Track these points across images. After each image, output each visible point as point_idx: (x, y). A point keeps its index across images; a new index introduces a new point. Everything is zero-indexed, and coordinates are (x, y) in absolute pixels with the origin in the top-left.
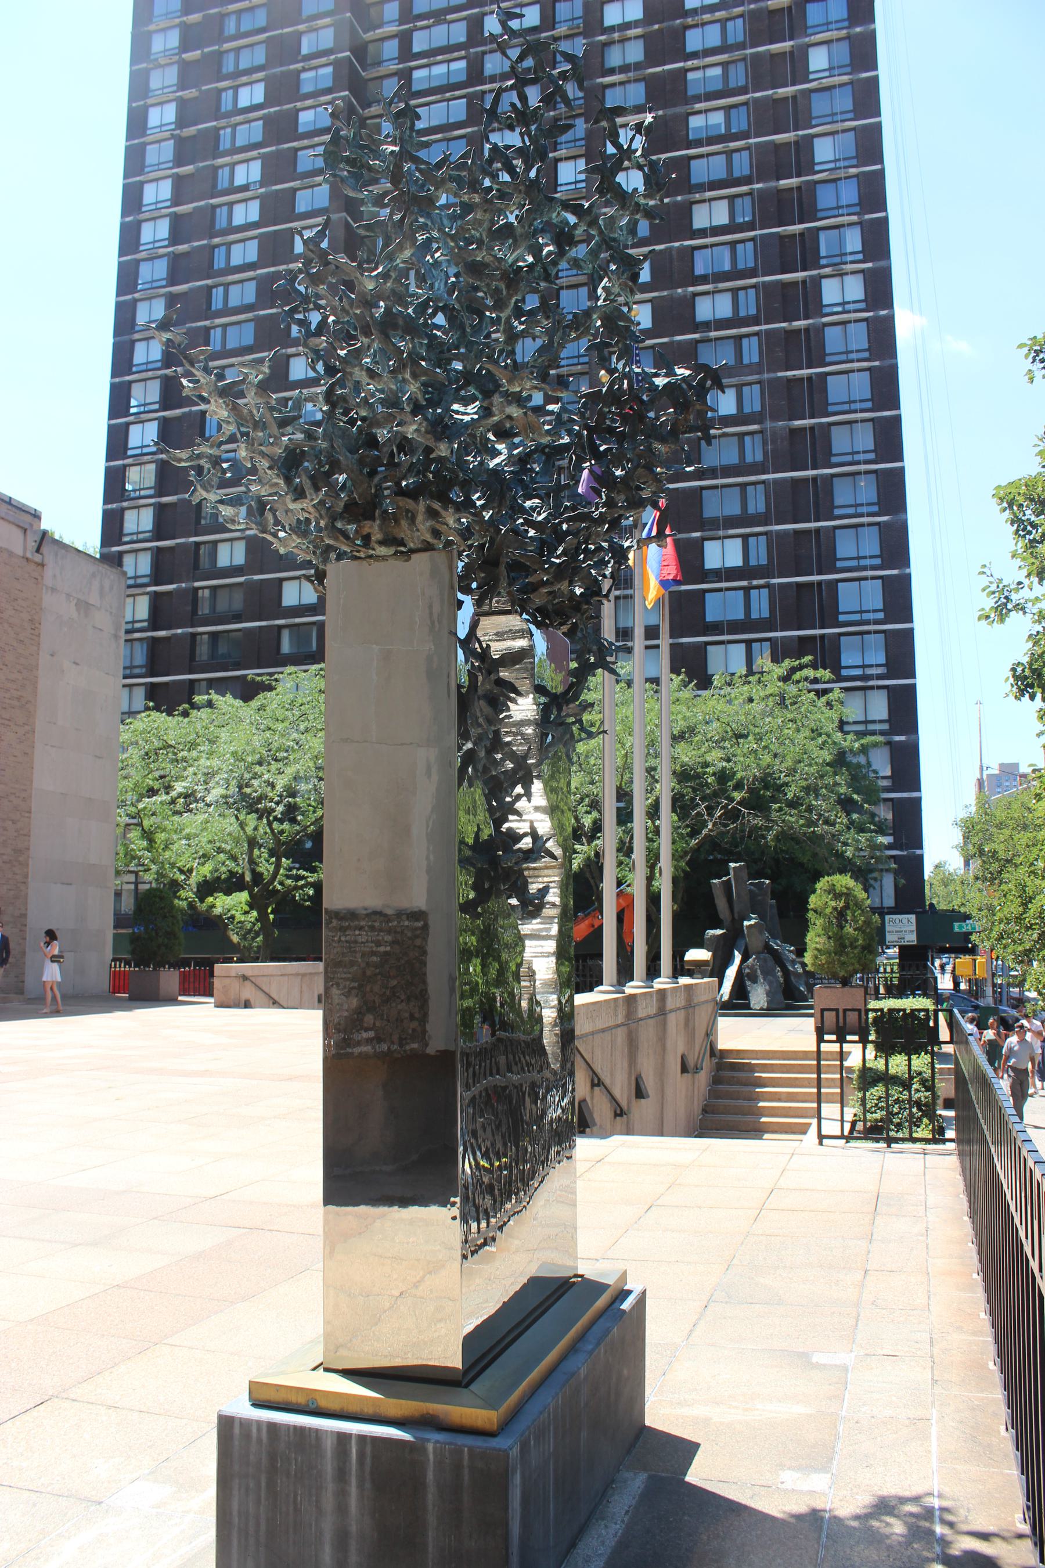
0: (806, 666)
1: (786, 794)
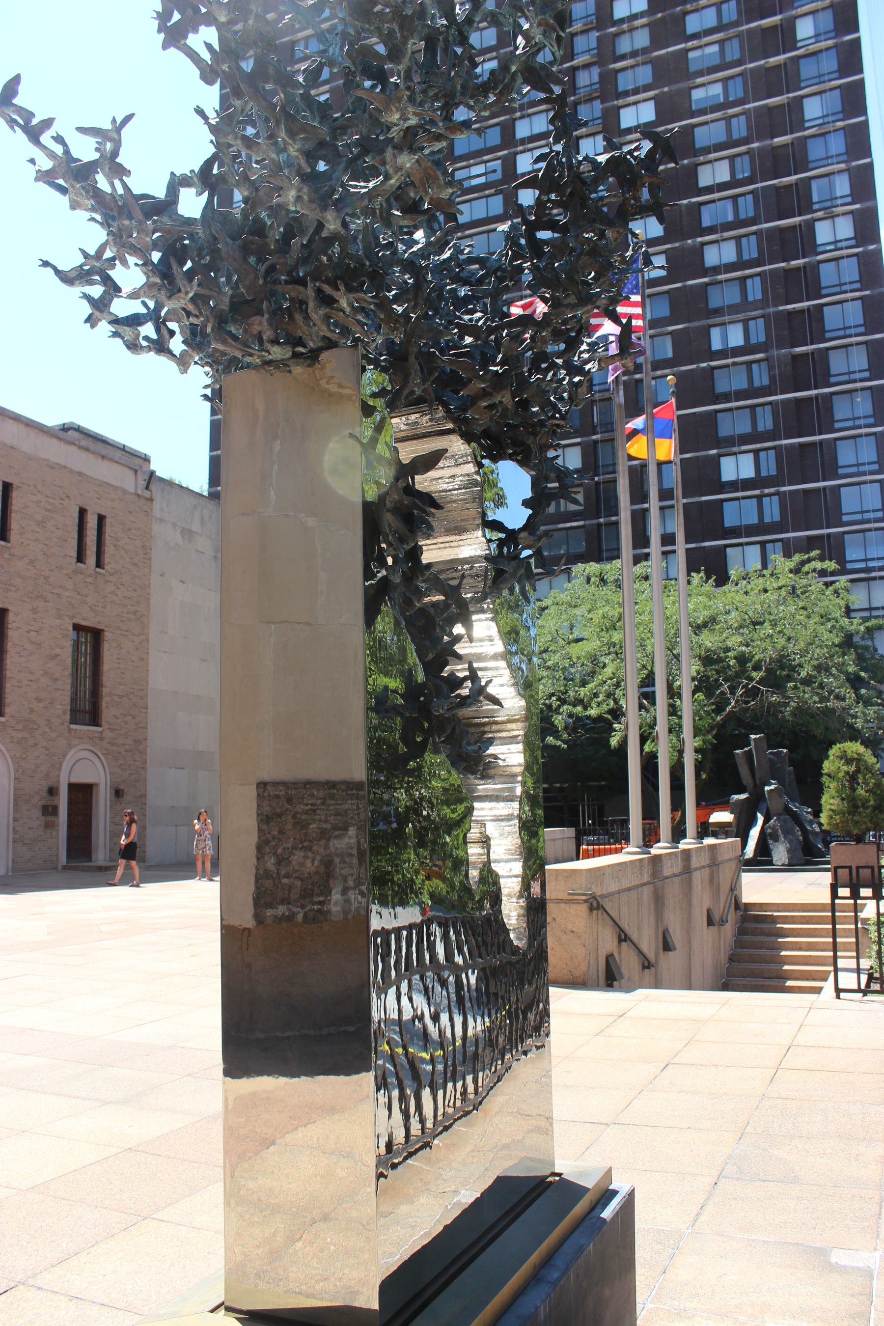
0: (814, 559)
1: (799, 674)
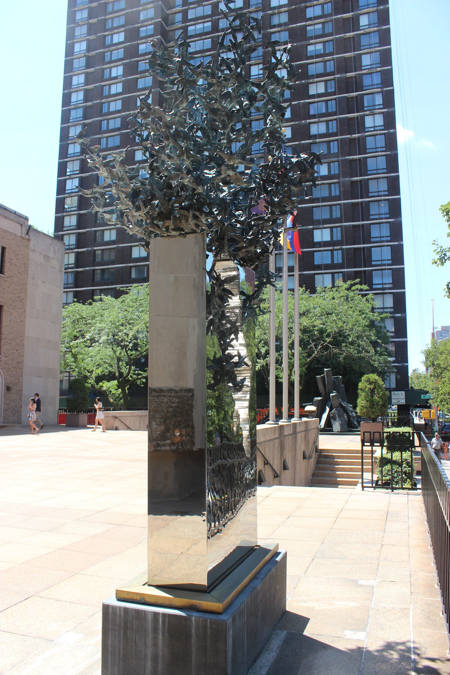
1: (348, 339)
